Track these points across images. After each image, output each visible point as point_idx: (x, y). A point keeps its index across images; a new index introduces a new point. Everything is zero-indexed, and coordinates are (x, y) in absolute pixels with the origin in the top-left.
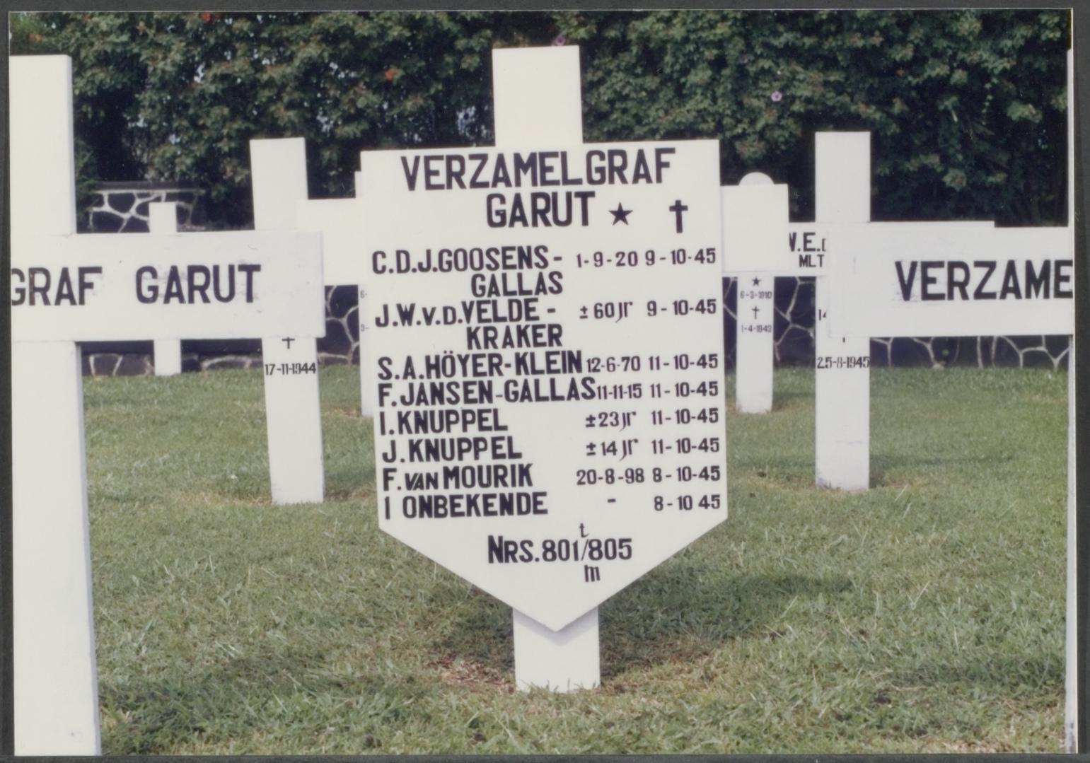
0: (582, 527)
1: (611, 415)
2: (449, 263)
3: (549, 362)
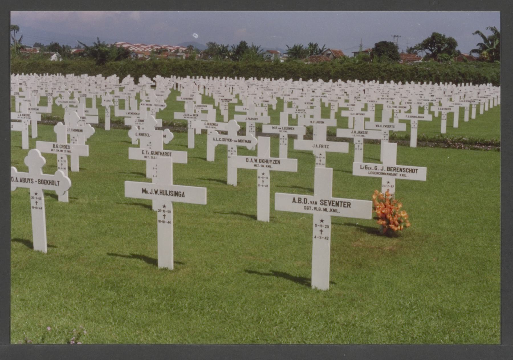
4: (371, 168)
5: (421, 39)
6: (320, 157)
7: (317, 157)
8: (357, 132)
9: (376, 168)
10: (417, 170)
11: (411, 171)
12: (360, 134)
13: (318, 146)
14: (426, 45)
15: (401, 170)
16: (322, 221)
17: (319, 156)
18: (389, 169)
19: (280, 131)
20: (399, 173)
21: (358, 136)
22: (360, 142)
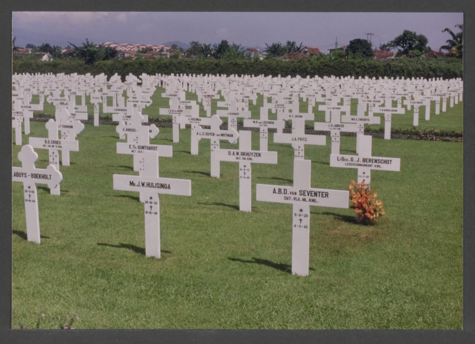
4: (347, 160)
5: (393, 38)
7: (296, 150)
8: (334, 125)
9: (352, 159)
10: (391, 161)
12: (337, 128)
13: (297, 139)
14: (398, 42)
15: (376, 161)
17: (297, 148)
18: (365, 160)
19: (261, 125)
20: (374, 164)
21: (334, 129)
22: (304, 213)
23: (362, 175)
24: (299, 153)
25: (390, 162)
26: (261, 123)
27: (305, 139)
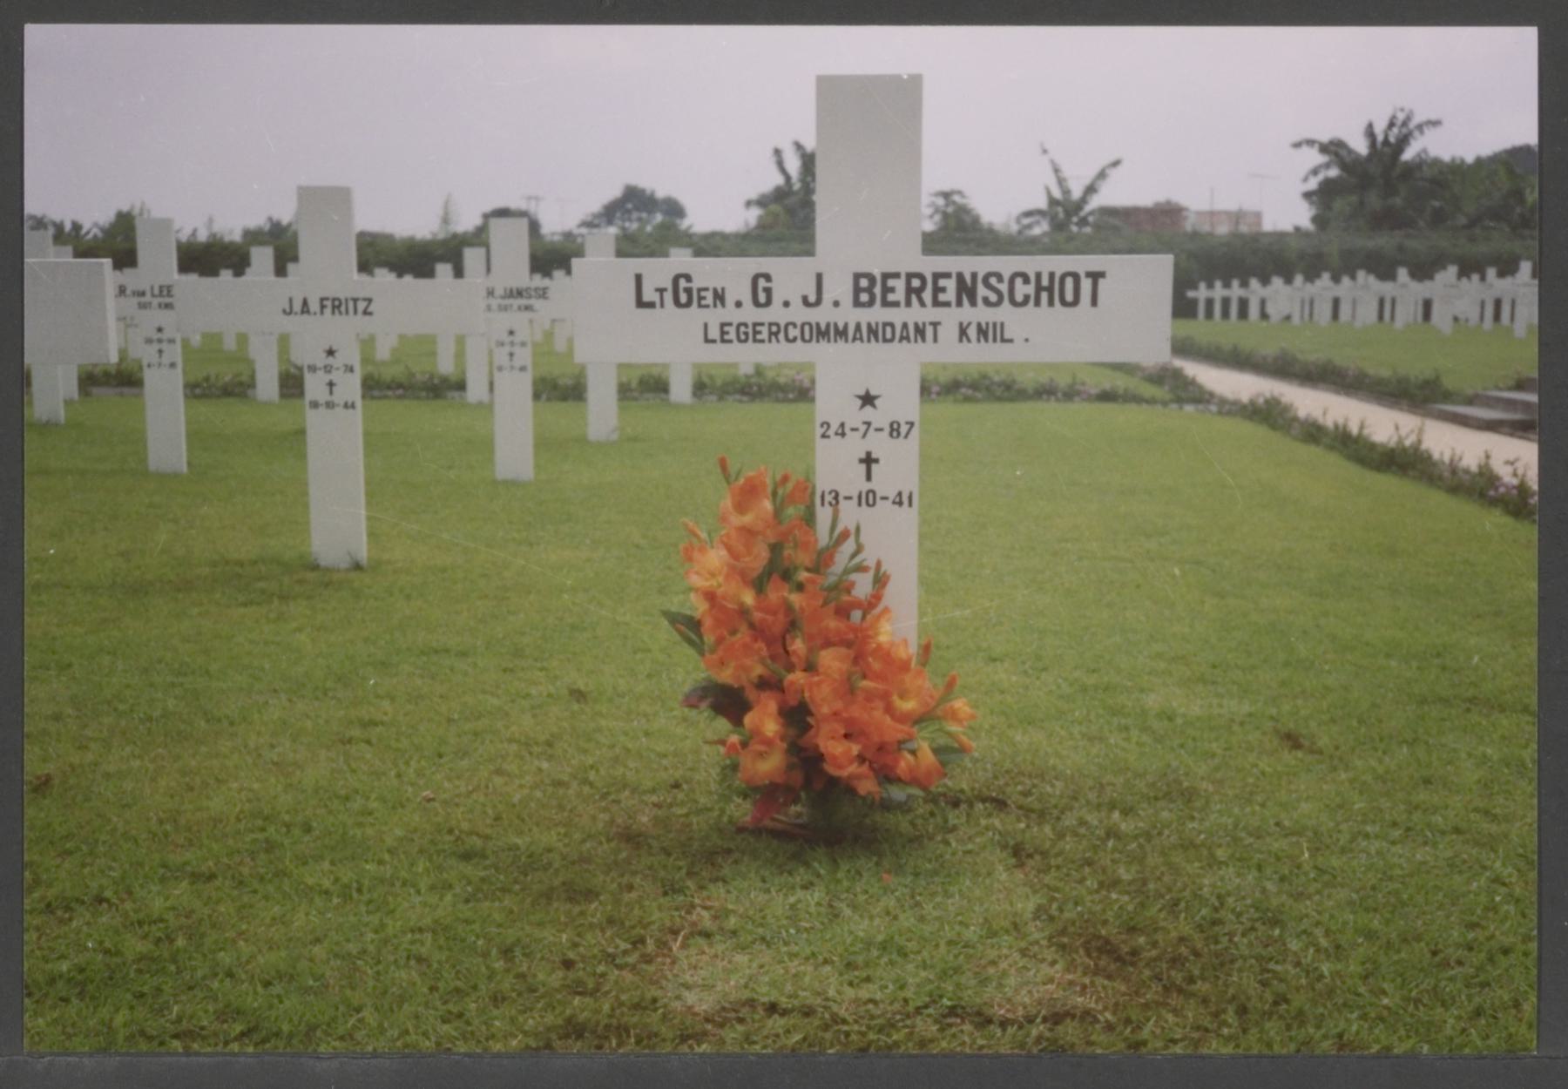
0: (1116, 164)
1: (795, 339)
2: (746, 334)
3: (723, 333)
4: (719, 297)
5: (595, 203)
6: (328, 369)
7: (313, 369)
8: (499, 292)
10: (1096, 276)
11: (1050, 291)
13: (314, 306)
14: (610, 212)
15: (967, 291)
16: (331, 353)
17: (321, 360)
18: (867, 288)
19: (142, 306)
20: (950, 318)
21: (504, 308)
22: (518, 338)
23: (855, 415)
24: (331, 384)
25: (1086, 285)
26: (143, 294)
27: (361, 306)
